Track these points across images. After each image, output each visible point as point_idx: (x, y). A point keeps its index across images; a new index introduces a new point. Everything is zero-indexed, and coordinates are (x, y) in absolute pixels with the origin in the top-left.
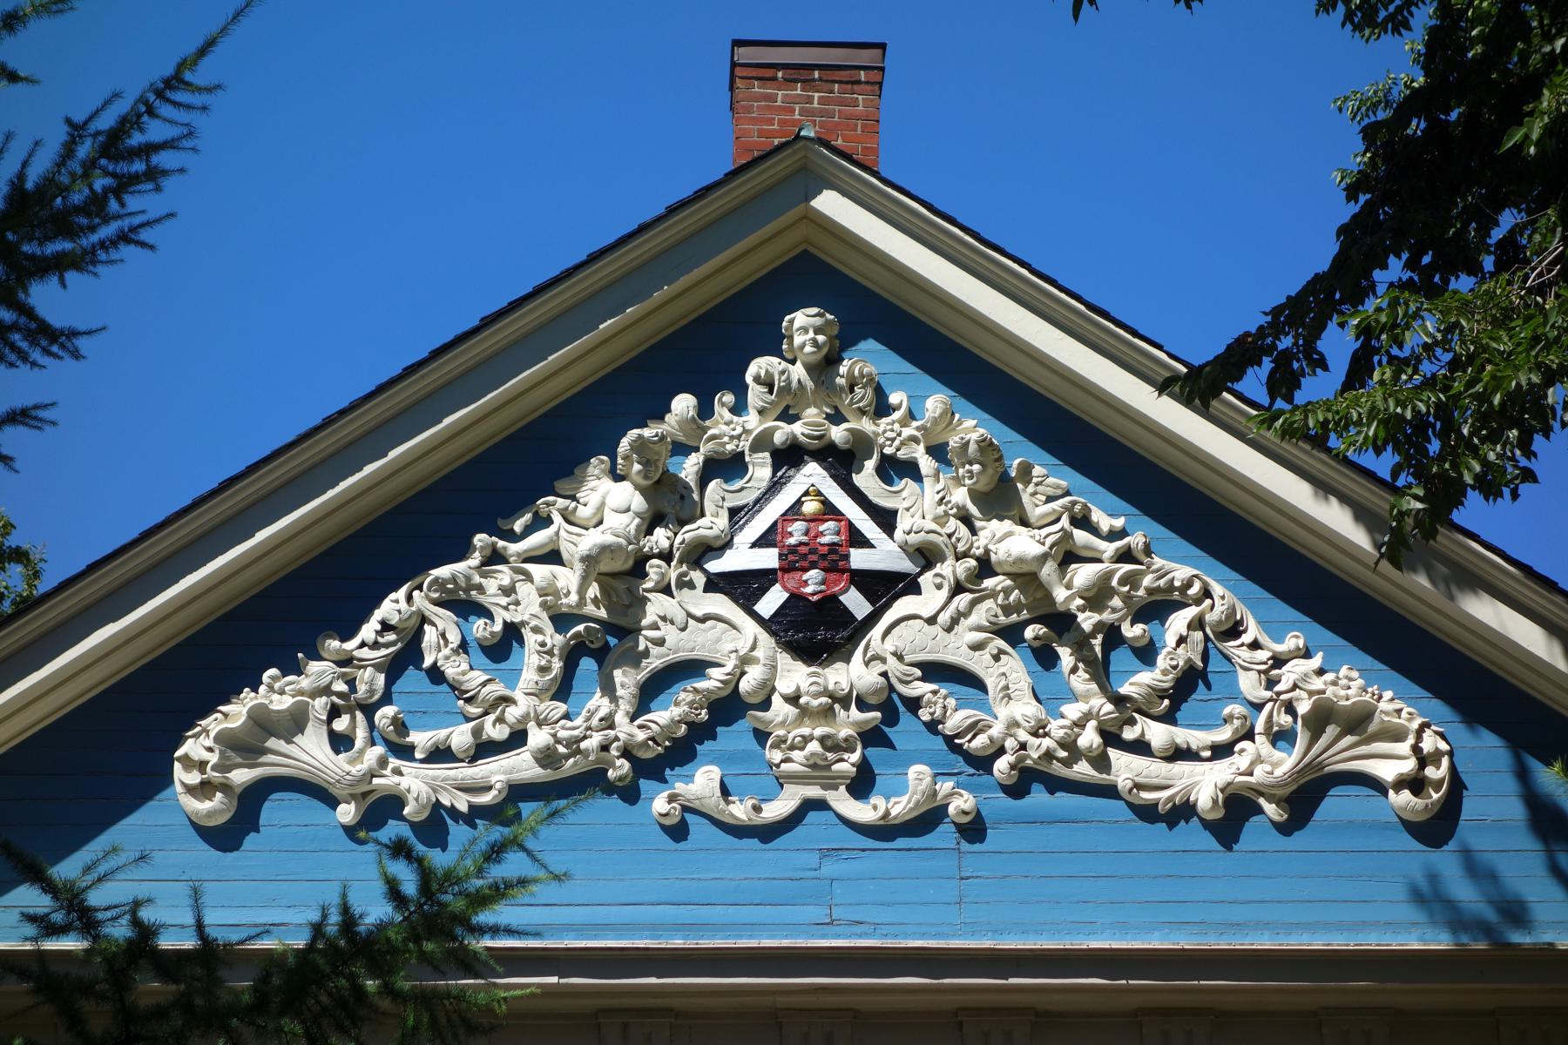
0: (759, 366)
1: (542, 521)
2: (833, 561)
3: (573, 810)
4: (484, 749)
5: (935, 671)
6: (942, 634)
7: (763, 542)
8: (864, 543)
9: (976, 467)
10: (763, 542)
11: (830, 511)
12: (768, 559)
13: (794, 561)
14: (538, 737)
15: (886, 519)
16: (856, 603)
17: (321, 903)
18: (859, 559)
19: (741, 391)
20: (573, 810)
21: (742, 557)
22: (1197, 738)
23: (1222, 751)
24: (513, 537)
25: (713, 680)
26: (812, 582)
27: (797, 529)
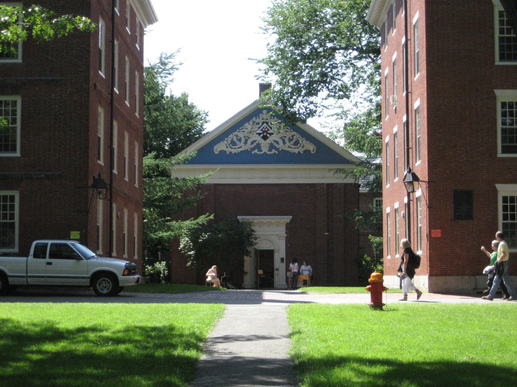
0: (261, 115)
1: (243, 128)
2: (267, 132)
3: (172, 81)
4: (239, 148)
5: (275, 141)
6: (358, 101)
7: (261, 130)
8: (269, 130)
9: (200, 191)
10: (261, 130)
11: (266, 128)
12: (261, 132)
13: (264, 132)
14: (243, 147)
15: (271, 128)
16: (268, 135)
17: (260, 143)
18: (269, 132)
19: (259, 117)
20: (172, 81)
21: (259, 131)
22: (296, 147)
23: (298, 148)
24: (240, 130)
25: (257, 142)
26: (265, 134)
27: (264, 129)
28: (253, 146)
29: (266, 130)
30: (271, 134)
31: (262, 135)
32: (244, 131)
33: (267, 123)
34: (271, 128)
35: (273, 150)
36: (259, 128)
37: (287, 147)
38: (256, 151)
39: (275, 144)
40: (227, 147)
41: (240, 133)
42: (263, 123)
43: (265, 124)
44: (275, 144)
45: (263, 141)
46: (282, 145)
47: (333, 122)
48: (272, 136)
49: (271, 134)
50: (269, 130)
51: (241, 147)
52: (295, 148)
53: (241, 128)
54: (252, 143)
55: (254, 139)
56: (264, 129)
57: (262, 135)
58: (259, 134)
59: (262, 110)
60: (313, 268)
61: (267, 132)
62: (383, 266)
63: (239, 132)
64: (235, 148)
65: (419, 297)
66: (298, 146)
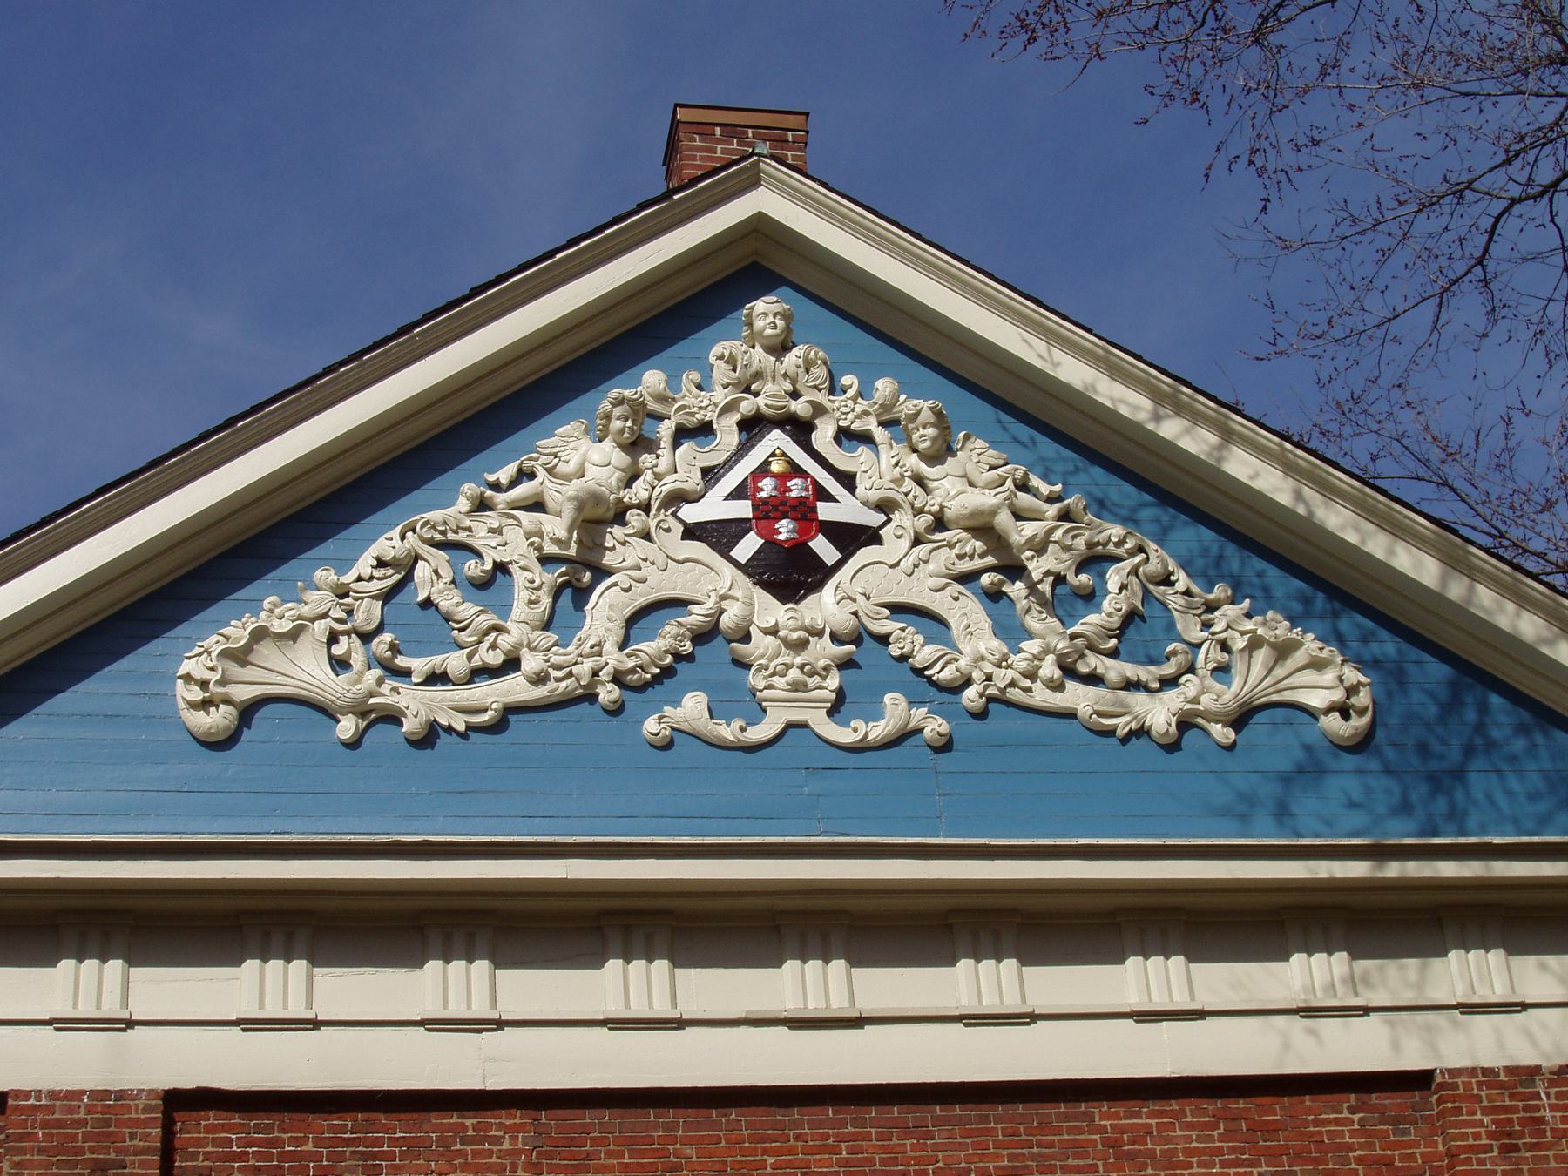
2: (803, 512)
7: (738, 493)
8: (828, 497)
10: (738, 493)
11: (796, 470)
12: (743, 509)
13: (767, 512)
14: (531, 663)
16: (823, 548)
18: (825, 511)
21: (715, 507)
23: (1169, 682)
26: (785, 529)
28: (655, 646)
29: (796, 487)
30: (851, 538)
31: (748, 546)
32: (537, 505)
33: (801, 429)
34: (848, 481)
35: (894, 703)
36: (710, 475)
37: (1049, 669)
38: (692, 708)
39: (906, 638)
40: (340, 664)
41: (492, 518)
42: (753, 427)
43: (776, 439)
44: (906, 638)
45: (770, 610)
46: (991, 645)
47: (1322, 353)
48: (865, 554)
49: (851, 538)
50: (828, 497)
51: (512, 664)
52: (1131, 685)
53: (504, 475)
54: (639, 620)
55: (661, 585)
56: (767, 487)
57: (748, 546)
58: (720, 535)
59: (1161, 687)
60: (484, 472)
61: (803, 512)
62: (1436, 1069)
63: (482, 505)
64: (436, 678)
65: (864, 472)
66: (1168, 669)
